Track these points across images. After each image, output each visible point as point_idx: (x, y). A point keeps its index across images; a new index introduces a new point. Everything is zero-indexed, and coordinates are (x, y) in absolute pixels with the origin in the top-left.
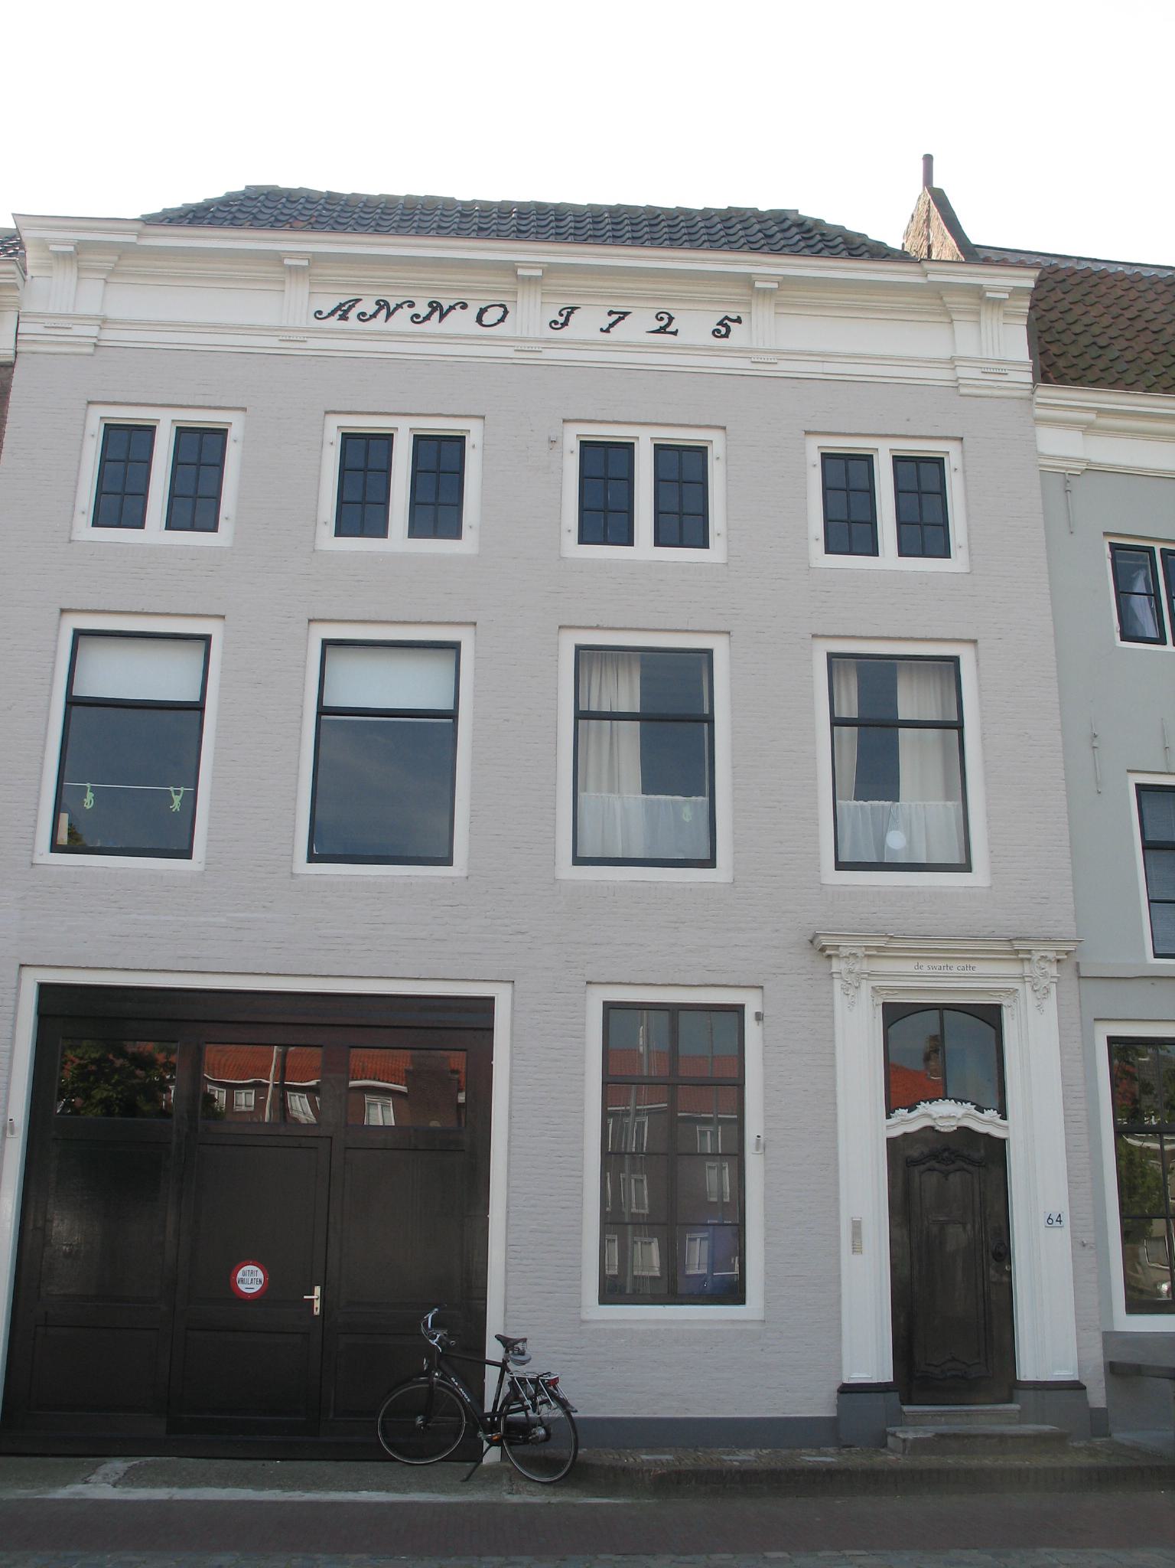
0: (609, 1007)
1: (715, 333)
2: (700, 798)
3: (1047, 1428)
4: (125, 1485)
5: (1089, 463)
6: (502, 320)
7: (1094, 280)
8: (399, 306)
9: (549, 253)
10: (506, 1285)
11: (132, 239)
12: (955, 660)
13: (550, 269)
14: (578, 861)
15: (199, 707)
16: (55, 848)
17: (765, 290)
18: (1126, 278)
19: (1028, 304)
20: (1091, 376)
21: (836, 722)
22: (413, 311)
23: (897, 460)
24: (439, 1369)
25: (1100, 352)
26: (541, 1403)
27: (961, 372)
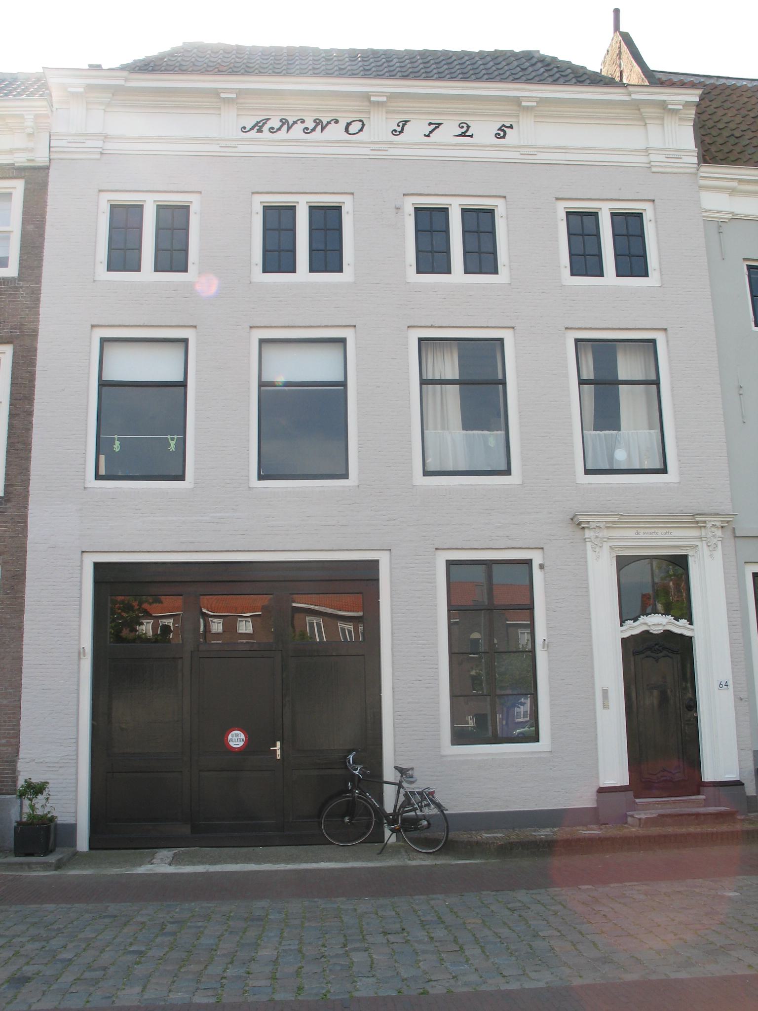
0: (450, 563)
1: (497, 136)
2: (499, 432)
3: (723, 809)
4: (177, 864)
5: (733, 214)
6: (361, 130)
7: (727, 92)
8: (295, 123)
9: (408, 86)
10: (395, 736)
11: (122, 82)
12: (653, 341)
13: (392, 96)
14: (426, 473)
15: (183, 385)
16: (98, 477)
17: (528, 107)
18: (749, 89)
19: (694, 112)
20: (732, 157)
21: (582, 382)
22: (304, 126)
23: (613, 215)
24: (358, 788)
25: (737, 141)
26: (426, 806)
27: (653, 157)
